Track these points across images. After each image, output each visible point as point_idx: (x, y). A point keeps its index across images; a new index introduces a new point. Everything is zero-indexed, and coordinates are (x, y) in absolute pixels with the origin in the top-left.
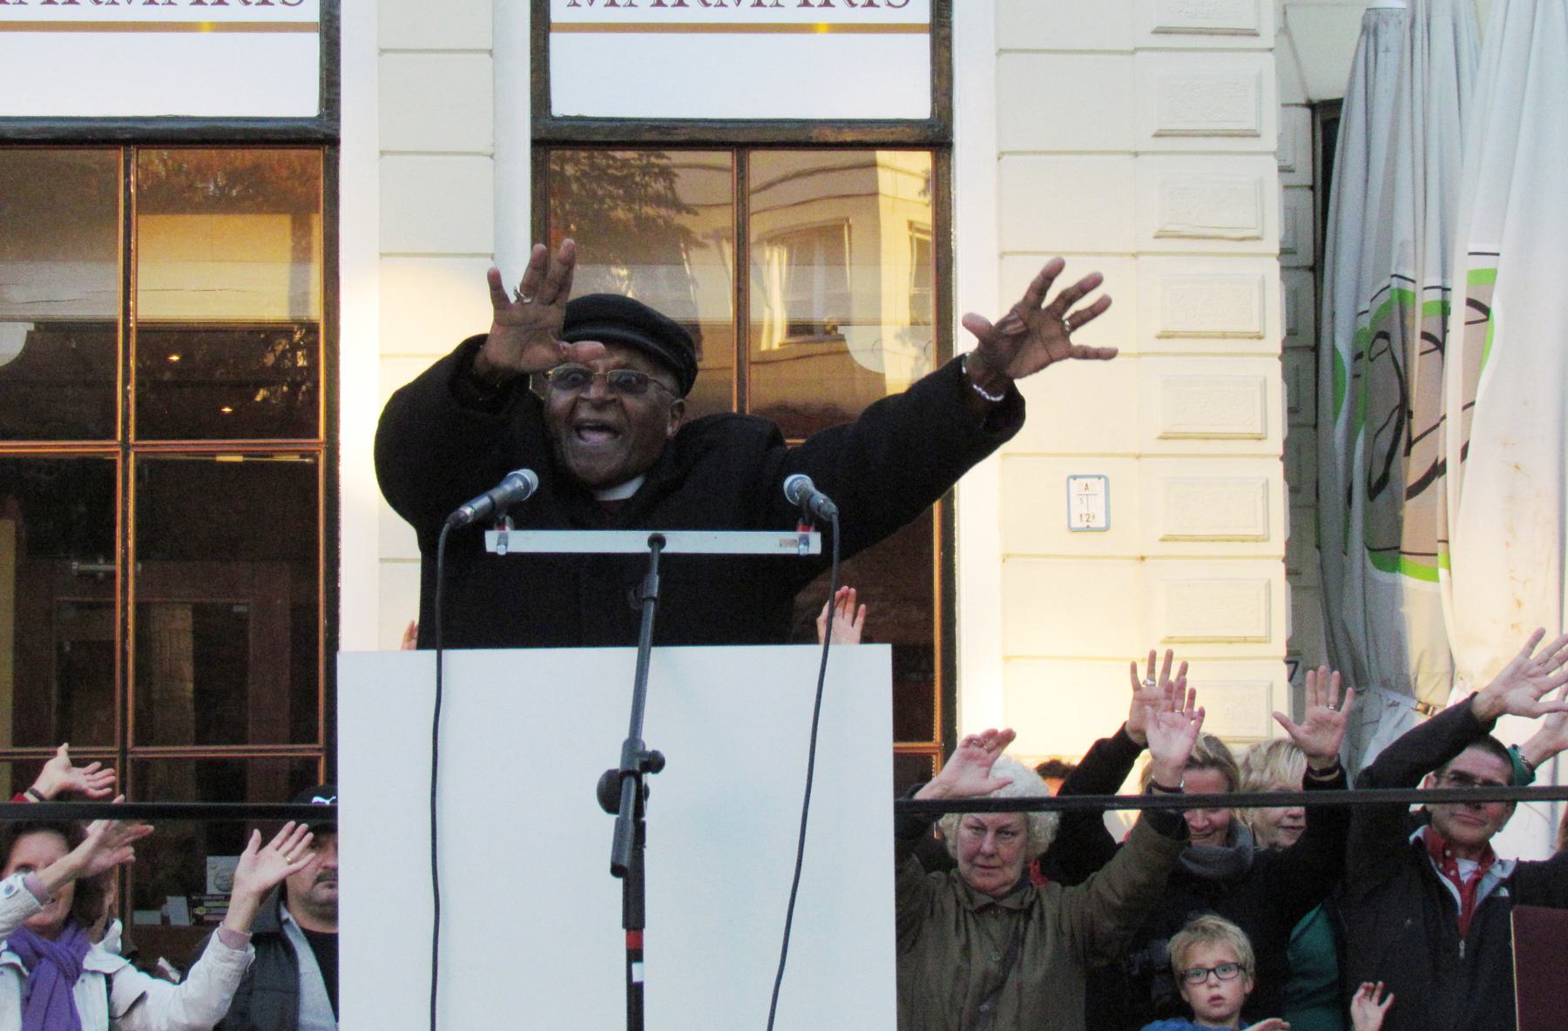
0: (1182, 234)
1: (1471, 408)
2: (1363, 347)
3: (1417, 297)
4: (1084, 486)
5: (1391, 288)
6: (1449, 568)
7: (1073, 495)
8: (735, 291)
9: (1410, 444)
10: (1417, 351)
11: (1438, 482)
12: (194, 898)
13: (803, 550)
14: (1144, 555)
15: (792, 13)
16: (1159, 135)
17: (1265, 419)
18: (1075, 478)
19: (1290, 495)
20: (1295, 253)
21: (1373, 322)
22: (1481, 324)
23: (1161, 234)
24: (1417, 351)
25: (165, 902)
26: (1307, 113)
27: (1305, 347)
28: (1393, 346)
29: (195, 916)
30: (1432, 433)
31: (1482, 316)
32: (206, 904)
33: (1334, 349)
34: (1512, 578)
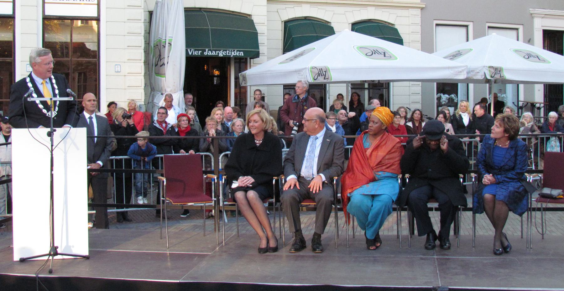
9: (161, 60)
13: (71, 100)
15: (78, 2)
16: (128, 20)
21: (156, 43)
26: (148, 12)
33: (151, 45)
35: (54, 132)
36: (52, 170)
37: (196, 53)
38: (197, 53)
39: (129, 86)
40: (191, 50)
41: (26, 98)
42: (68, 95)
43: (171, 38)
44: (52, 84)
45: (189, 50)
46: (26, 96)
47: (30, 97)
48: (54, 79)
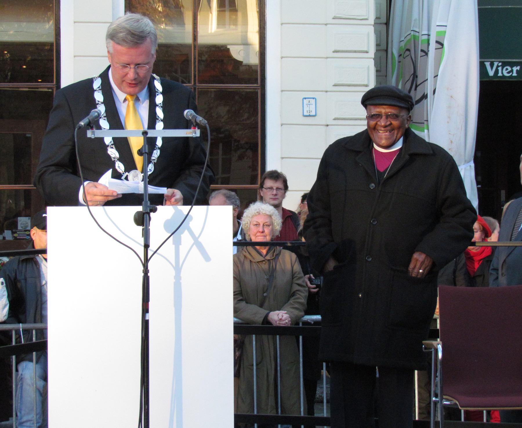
0: (342, 17)
1: (436, 77)
2: (402, 53)
3: (420, 37)
4: (308, 101)
5: (411, 34)
6: (428, 130)
7: (304, 104)
8: (193, 40)
9: (416, 87)
10: (419, 56)
11: (424, 101)
12: (14, 231)
13: (194, 135)
14: (328, 124)
17: (368, 47)
18: (305, 98)
19: (376, 73)
20: (380, 45)
21: (405, 45)
22: (441, 49)
23: (335, 17)
24: (419, 56)
25: (4, 232)
27: (383, 50)
28: (411, 54)
29: (14, 237)
30: (423, 83)
31: (441, 47)
32: (18, 233)
34: (449, 133)
35: (152, 214)
36: (145, 310)
37: (505, 72)
38: (508, 73)
39: (338, 16)
40: (492, 65)
41: (83, 131)
42: (187, 124)
43: (442, 29)
44: (153, 106)
45: (488, 64)
46: (82, 123)
47: (92, 128)
48: (163, 93)
